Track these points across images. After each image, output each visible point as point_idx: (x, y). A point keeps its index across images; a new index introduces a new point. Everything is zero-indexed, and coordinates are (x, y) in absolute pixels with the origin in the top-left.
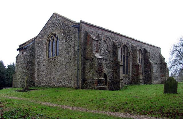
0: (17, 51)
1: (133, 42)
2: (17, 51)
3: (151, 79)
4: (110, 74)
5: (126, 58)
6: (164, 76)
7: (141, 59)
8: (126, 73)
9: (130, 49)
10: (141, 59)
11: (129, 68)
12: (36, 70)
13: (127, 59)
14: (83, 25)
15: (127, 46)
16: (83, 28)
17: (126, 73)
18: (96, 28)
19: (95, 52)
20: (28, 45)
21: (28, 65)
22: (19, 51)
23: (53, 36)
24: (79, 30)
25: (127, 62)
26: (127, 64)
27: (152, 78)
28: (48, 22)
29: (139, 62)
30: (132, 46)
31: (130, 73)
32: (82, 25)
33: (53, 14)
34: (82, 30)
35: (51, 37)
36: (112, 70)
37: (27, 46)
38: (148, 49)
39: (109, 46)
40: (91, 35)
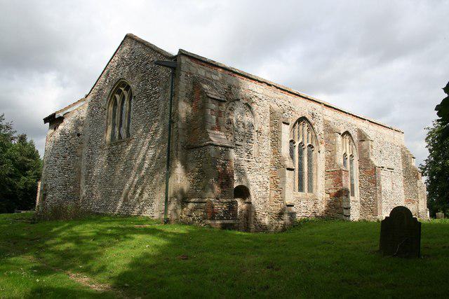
0: (45, 123)
1: (328, 112)
2: (45, 123)
3: (376, 207)
4: (259, 190)
5: (306, 150)
6: (413, 203)
7: (349, 155)
8: (306, 189)
10: (349, 155)
11: (314, 176)
12: (84, 171)
13: (309, 155)
14: (184, 60)
15: (309, 122)
16: (184, 68)
17: (306, 189)
18: (258, 83)
20: (68, 111)
21: (65, 157)
23: (122, 89)
24: (174, 75)
25: (310, 161)
28: (116, 52)
29: (292, 157)
31: (319, 191)
32: (183, 61)
33: (126, 36)
34: (183, 74)
35: (119, 92)
36: (266, 179)
37: (65, 112)
38: (114, 77)
40: (205, 86)
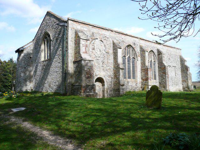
0: (16, 53)
2: (16, 53)
4: (108, 79)
7: (153, 61)
9: (138, 50)
10: (153, 61)
17: (132, 78)
19: (84, 53)
22: (17, 53)
26: (133, 67)
27: (167, 84)
30: (140, 46)
33: (47, 12)
39: (107, 46)
